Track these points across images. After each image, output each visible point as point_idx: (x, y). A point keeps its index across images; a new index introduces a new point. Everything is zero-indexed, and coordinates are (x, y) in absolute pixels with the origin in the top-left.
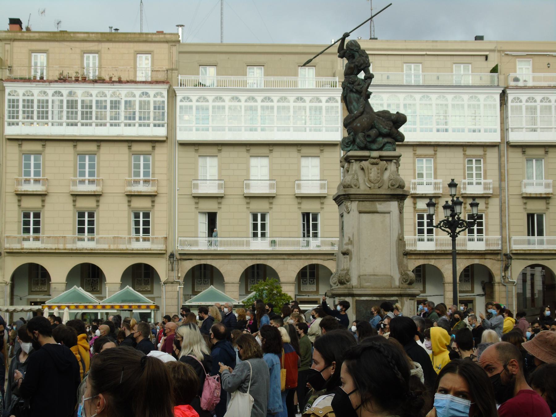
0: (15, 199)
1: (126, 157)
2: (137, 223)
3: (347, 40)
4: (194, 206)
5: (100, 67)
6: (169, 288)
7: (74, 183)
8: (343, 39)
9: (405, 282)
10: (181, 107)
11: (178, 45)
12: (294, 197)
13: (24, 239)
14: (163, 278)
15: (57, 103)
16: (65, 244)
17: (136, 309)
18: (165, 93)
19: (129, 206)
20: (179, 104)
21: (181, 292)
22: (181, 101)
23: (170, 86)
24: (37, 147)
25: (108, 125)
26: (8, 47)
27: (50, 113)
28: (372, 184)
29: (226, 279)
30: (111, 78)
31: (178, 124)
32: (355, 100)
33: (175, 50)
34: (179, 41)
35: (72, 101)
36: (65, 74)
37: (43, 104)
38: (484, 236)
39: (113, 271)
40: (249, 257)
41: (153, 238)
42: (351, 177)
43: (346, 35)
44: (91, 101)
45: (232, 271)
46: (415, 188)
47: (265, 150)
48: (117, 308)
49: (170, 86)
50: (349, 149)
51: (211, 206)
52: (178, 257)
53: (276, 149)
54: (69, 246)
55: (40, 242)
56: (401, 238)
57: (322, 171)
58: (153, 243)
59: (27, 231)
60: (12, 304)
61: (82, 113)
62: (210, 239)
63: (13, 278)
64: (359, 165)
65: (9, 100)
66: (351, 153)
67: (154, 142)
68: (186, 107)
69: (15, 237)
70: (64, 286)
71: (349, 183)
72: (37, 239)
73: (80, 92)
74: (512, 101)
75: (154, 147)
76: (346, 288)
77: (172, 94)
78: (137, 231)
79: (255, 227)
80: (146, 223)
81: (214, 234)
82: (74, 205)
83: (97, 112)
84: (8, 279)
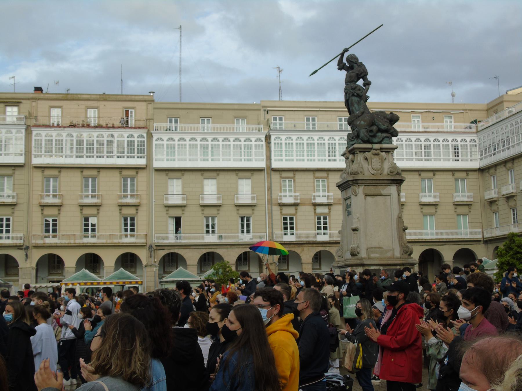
0: (39, 209)
1: (118, 179)
2: (126, 225)
3: (346, 55)
4: (165, 213)
5: (99, 117)
6: (149, 269)
7: (81, 197)
8: (342, 54)
9: (406, 253)
10: (156, 145)
11: (152, 103)
12: (234, 205)
13: (46, 237)
14: (144, 263)
15: (69, 142)
16: (75, 240)
17: (129, 284)
18: (145, 135)
19: (120, 213)
20: (154, 142)
21: (157, 272)
22: (156, 140)
23: (149, 131)
24: (55, 172)
25: (105, 157)
26: (34, 104)
27: (64, 149)
28: (375, 172)
29: (188, 262)
30: (107, 125)
31: (154, 157)
32: (356, 103)
33: (151, 106)
34: (153, 101)
35: (80, 140)
36: (74, 123)
37: (59, 142)
38: (295, 232)
39: (109, 258)
40: (203, 247)
41: (137, 235)
42: (357, 165)
43: (346, 50)
44: (93, 141)
45: (192, 257)
46: (281, 199)
47: (214, 174)
48: (115, 283)
49: (149, 131)
50: (353, 142)
51: (177, 213)
52: (155, 248)
53: (221, 173)
54: (78, 241)
55: (57, 238)
56: (400, 216)
57: (253, 188)
58: (137, 238)
59: (47, 231)
60: (36, 282)
61: (87, 148)
62: (177, 235)
63: (37, 265)
64: (363, 156)
65: (35, 140)
66: (356, 146)
67: (137, 169)
68: (160, 145)
69: (39, 235)
70: (74, 270)
71: (356, 170)
72: (54, 237)
73: (85, 134)
74: (35, 136)
75: (137, 172)
76: (358, 259)
77: (150, 136)
78: (126, 230)
79: (208, 226)
80: (132, 225)
81: (179, 232)
82: (81, 213)
83: (97, 148)
84: (34, 265)
